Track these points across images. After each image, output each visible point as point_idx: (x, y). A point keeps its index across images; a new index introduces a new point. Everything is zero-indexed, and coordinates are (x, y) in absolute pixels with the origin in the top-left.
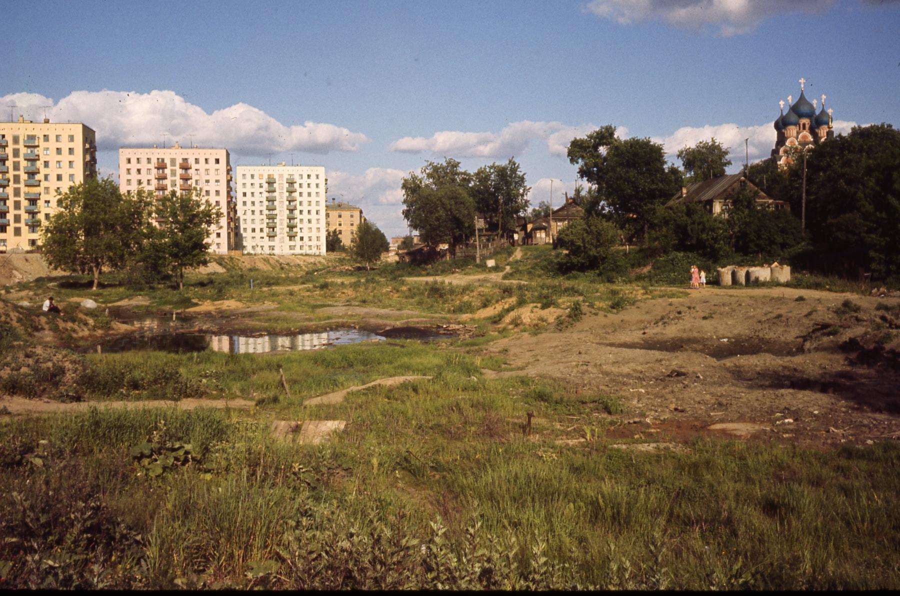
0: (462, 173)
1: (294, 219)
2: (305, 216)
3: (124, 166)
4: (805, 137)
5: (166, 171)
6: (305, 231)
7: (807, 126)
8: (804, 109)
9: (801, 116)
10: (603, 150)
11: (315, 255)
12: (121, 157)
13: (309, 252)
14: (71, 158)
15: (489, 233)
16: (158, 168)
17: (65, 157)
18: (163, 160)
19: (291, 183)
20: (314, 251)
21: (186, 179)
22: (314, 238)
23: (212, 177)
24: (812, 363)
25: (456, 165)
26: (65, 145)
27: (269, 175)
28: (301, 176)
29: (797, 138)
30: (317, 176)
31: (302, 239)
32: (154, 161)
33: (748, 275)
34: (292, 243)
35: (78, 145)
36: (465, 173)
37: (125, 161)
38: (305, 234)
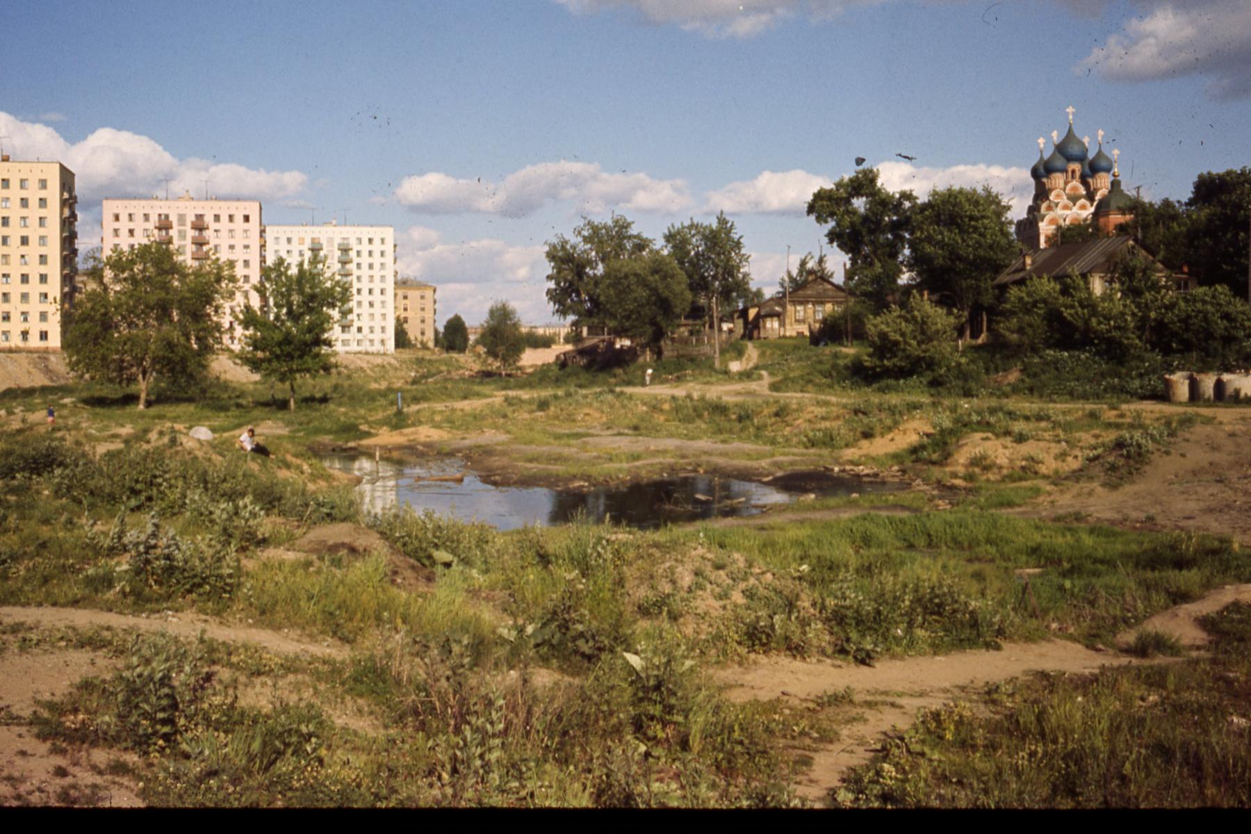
0: (635, 237)
3: (109, 224)
4: (1075, 188)
5: (171, 232)
6: (365, 317)
7: (1078, 174)
8: (1074, 150)
9: (1070, 159)
10: (860, 204)
11: (378, 354)
12: (105, 212)
13: (370, 349)
14: (43, 213)
15: (690, 322)
16: (160, 229)
17: (34, 212)
18: (167, 216)
19: (345, 250)
20: (377, 347)
21: (200, 243)
22: (377, 330)
23: (239, 242)
25: (627, 226)
26: (34, 194)
27: (313, 240)
28: (360, 241)
29: (1064, 190)
30: (383, 241)
31: (360, 330)
32: (154, 219)
33: (1219, 386)
35: (53, 193)
36: (638, 236)
37: (112, 218)
38: (365, 323)
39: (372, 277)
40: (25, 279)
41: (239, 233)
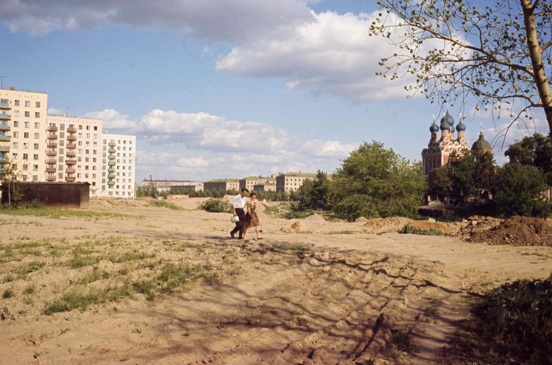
1: (113, 172)
2: (121, 171)
17: (32, 119)
18: (54, 125)
24: (224, 288)
26: (32, 110)
30: (130, 142)
31: (118, 187)
34: (111, 190)
38: (121, 184)
39: (125, 160)
40: (25, 156)
41: (92, 136)
